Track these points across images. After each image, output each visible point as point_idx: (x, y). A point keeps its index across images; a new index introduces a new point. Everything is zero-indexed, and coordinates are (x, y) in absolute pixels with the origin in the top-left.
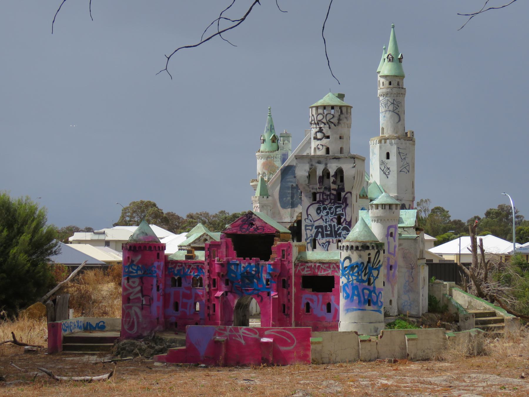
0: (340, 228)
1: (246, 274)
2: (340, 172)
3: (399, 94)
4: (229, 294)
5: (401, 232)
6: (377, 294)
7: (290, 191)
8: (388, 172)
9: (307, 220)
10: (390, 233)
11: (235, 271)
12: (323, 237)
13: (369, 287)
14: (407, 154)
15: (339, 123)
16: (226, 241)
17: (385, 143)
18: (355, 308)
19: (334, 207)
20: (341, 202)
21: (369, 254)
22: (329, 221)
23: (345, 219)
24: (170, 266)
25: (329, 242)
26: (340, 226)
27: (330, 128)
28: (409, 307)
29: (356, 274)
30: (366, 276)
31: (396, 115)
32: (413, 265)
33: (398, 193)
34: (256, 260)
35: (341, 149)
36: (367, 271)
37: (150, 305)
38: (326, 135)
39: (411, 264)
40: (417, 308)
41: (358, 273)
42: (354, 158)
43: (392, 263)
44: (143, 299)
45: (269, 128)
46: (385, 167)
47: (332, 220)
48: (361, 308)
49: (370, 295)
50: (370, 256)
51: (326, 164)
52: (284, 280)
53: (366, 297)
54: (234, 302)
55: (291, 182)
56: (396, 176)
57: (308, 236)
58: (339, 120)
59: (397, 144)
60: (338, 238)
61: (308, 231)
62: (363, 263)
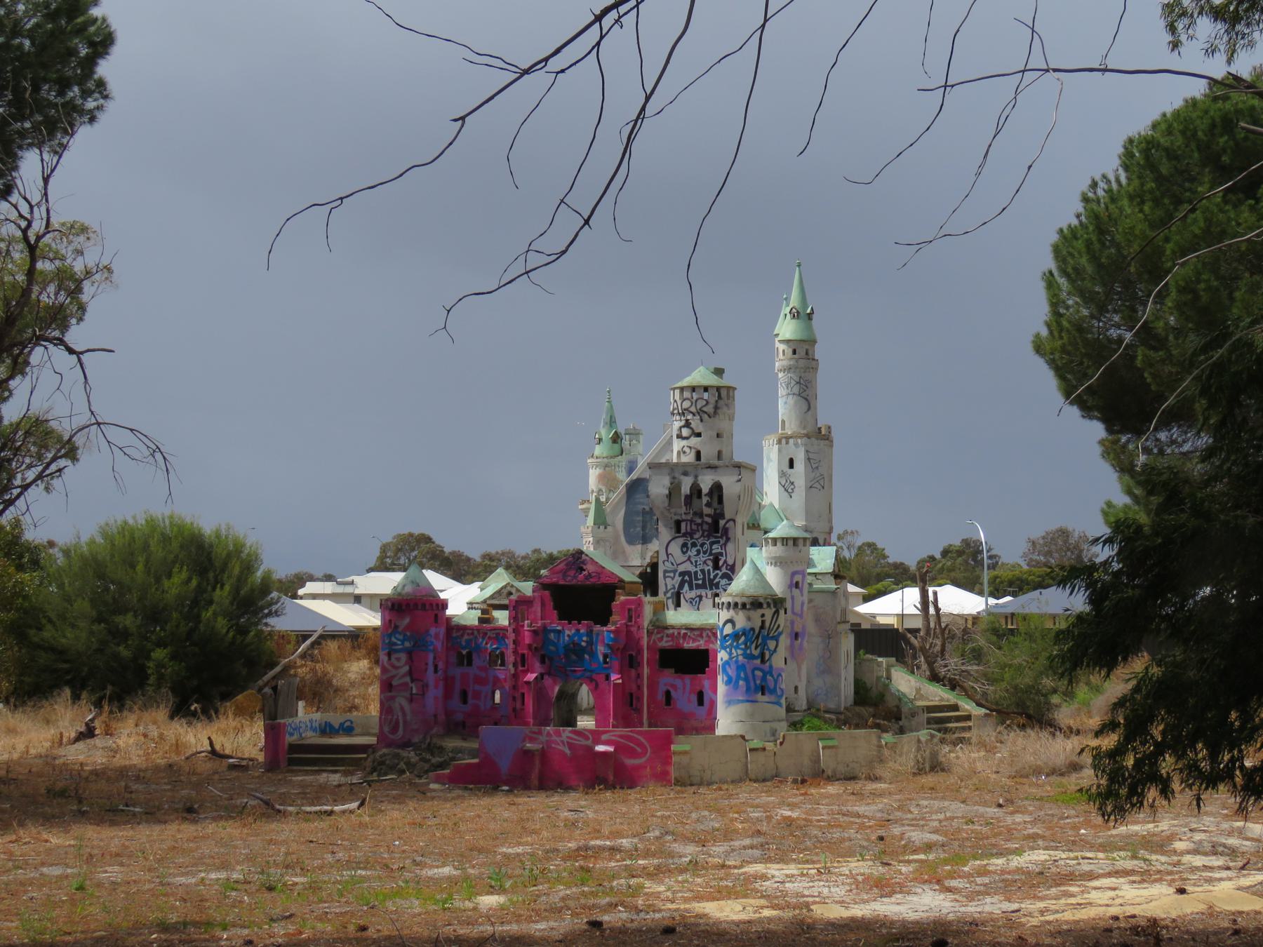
0: (717, 574)
2: (717, 489)
6: (775, 677)
9: (666, 563)
10: (794, 582)
12: (691, 588)
13: (762, 666)
15: (715, 413)
17: (787, 443)
18: (740, 698)
21: (763, 615)
23: (725, 562)
25: (700, 597)
26: (718, 572)
27: (702, 421)
29: (743, 646)
30: (759, 649)
34: (587, 624)
35: (720, 453)
36: (760, 641)
37: (424, 694)
38: (696, 431)
41: (746, 645)
43: (798, 628)
44: (413, 685)
48: (750, 699)
49: (764, 678)
51: (696, 477)
52: (631, 656)
53: (758, 682)
54: (553, 690)
57: (669, 588)
58: (716, 408)
61: (668, 580)
62: (753, 629)
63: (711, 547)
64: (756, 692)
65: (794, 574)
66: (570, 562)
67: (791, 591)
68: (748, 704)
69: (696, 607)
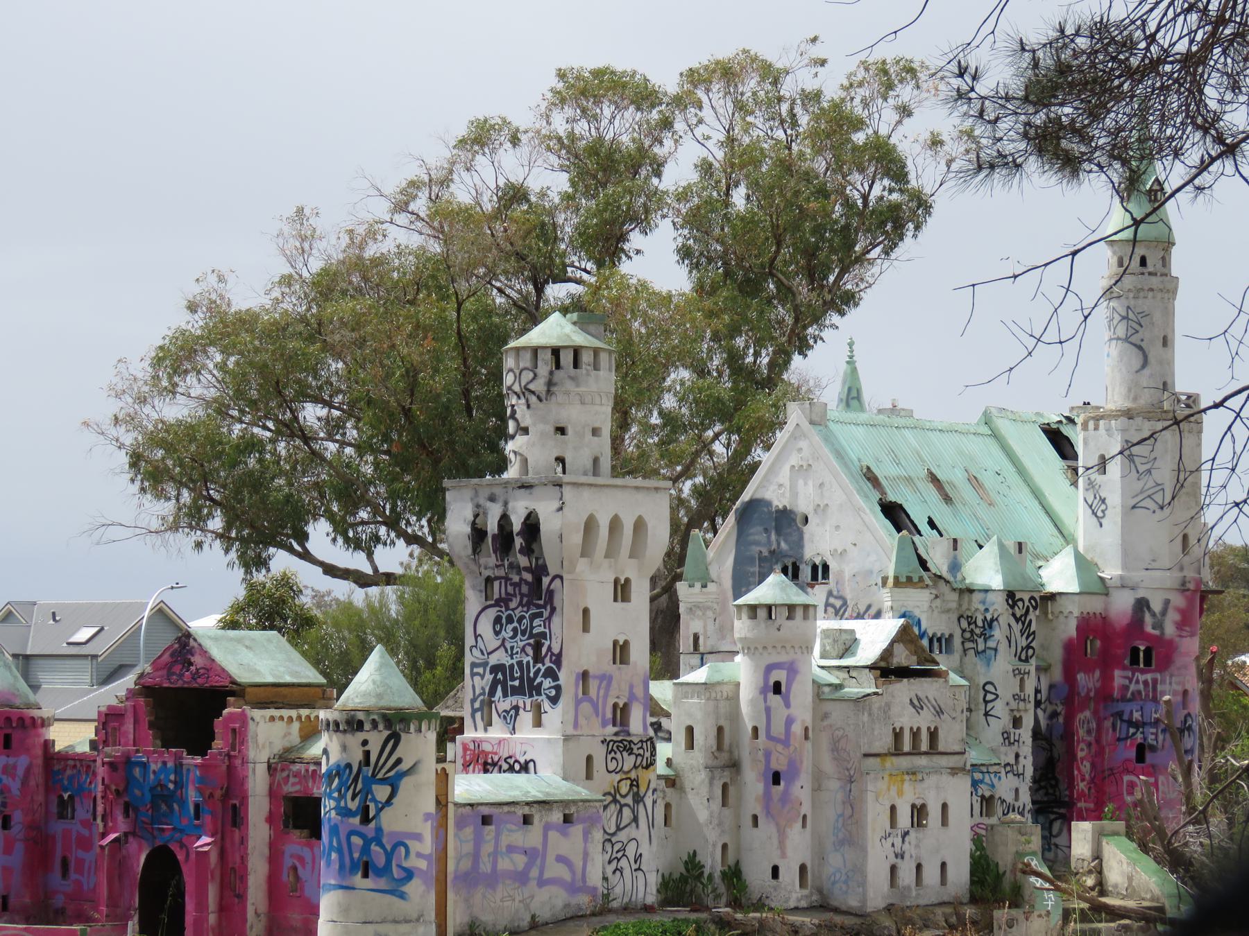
0: (539, 670)
1: (159, 789)
2: (532, 527)
3: (1142, 289)
4: (131, 839)
5: (844, 679)
6: (389, 848)
7: (757, 569)
8: (1103, 511)
9: (474, 649)
10: (771, 683)
11: (141, 780)
12: (505, 695)
13: (364, 829)
14: (1155, 459)
16: (134, 706)
17: (1096, 428)
18: (333, 882)
19: (527, 616)
20: (541, 602)
21: (365, 743)
22: (517, 653)
23: (549, 648)
24: (56, 768)
25: (516, 708)
26: (540, 665)
27: (528, 406)
28: (844, 888)
29: (336, 795)
30: (357, 800)
31: (1135, 350)
32: (852, 773)
33: (1125, 566)
34: (176, 753)
35: (561, 460)
36: (360, 786)
38: (522, 425)
39: (848, 770)
40: (861, 889)
41: (340, 791)
42: (561, 486)
43: (779, 764)
45: (844, 397)
46: (1095, 498)
47: (523, 650)
48: (344, 884)
49: (365, 849)
50: (366, 748)
51: (506, 504)
52: (234, 806)
53: (356, 855)
54: (138, 860)
55: (757, 543)
56: (1119, 520)
58: (550, 384)
59: (1124, 431)
60: (536, 698)
61: (477, 679)
62: (349, 766)
63: (531, 624)
64: (353, 870)
65: (769, 668)
66: (176, 650)
67: (765, 700)
68: (340, 891)
69: (511, 726)
